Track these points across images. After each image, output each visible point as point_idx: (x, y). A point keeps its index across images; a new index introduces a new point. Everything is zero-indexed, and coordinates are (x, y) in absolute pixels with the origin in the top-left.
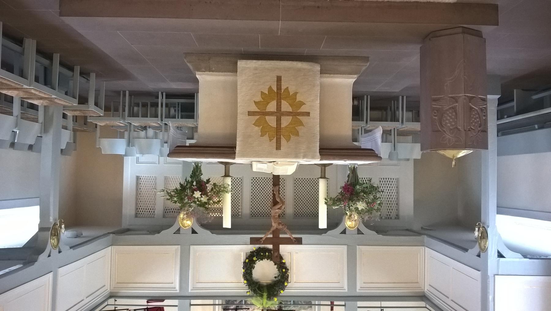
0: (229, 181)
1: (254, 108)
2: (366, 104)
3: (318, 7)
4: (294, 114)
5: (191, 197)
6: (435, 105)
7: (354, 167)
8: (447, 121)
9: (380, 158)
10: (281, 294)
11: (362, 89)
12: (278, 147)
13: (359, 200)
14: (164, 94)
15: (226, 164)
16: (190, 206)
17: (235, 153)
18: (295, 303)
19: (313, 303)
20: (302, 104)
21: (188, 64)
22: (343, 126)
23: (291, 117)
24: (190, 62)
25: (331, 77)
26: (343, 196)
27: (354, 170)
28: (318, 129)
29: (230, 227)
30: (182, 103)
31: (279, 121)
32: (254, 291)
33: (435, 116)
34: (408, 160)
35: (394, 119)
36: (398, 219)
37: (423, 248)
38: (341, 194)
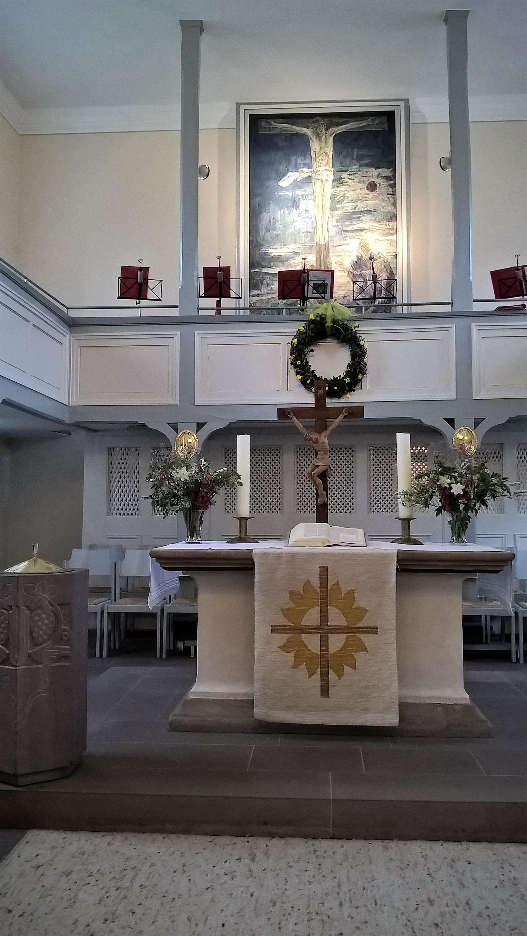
0: (403, 512)
1: (367, 639)
2: (163, 640)
3: (265, 823)
4: (297, 629)
5: (468, 483)
6: (65, 649)
7: (192, 537)
8: (46, 622)
9: (152, 555)
10: (303, 324)
11: (174, 670)
12: (324, 571)
13: (186, 483)
14: (514, 659)
15: (409, 541)
16: (468, 468)
17: (398, 561)
18: (279, 311)
19: (247, 312)
20: (284, 648)
21: (483, 717)
22: (212, 607)
23: (302, 624)
24: (482, 721)
25: (237, 694)
26: (212, 489)
27: (193, 532)
28: (256, 603)
29: (399, 435)
30: (481, 642)
31: (324, 616)
32: (347, 328)
33: (65, 630)
34: (92, 547)
35: (115, 617)
36: (109, 449)
37: (71, 404)
38: (213, 492)
